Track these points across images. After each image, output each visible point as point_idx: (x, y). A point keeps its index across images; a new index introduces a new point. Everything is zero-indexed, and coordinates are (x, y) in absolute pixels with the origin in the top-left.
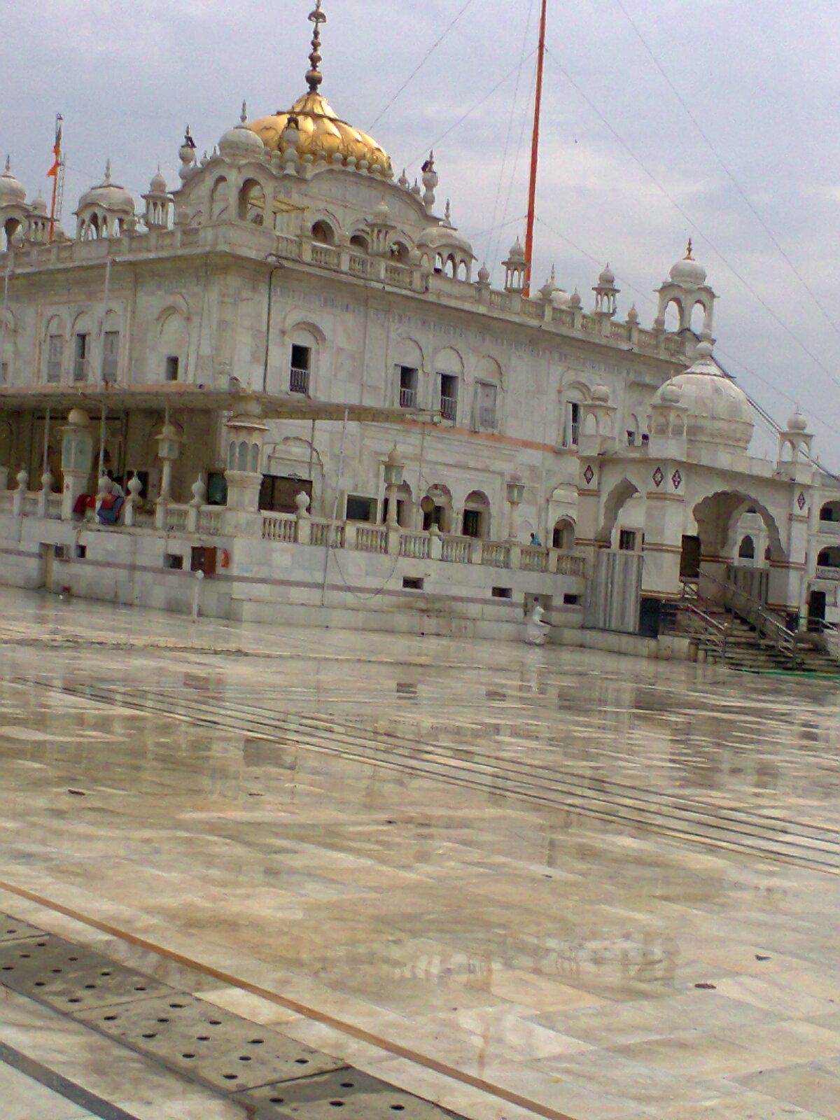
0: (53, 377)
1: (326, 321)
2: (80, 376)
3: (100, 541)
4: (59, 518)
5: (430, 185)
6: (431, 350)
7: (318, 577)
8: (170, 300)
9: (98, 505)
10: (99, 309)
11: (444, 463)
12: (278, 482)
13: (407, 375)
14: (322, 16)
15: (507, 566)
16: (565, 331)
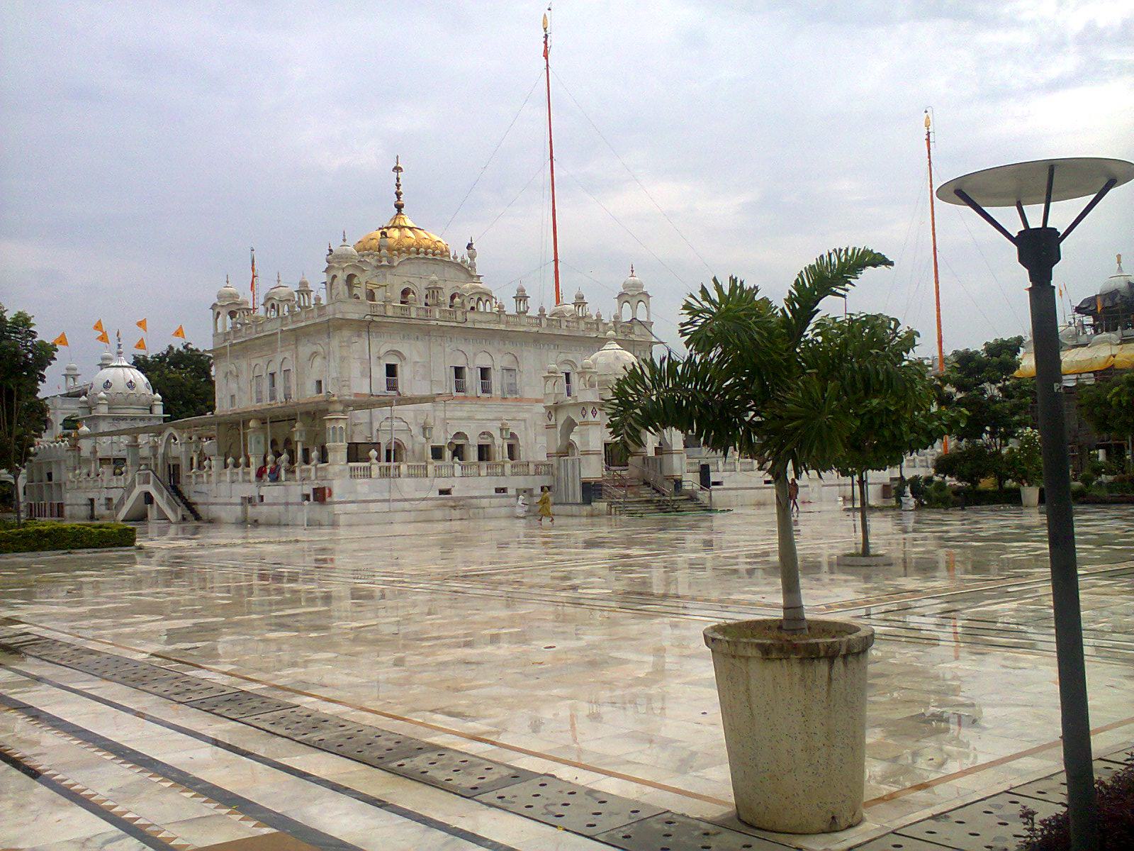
0: (259, 400)
1: (404, 348)
2: (273, 398)
3: (271, 491)
4: (250, 481)
5: (472, 257)
6: (472, 355)
7: (386, 496)
8: (314, 348)
9: (268, 471)
10: (279, 358)
11: (473, 420)
12: (359, 446)
13: (459, 372)
14: (401, 169)
15: (503, 475)
16: (556, 332)
